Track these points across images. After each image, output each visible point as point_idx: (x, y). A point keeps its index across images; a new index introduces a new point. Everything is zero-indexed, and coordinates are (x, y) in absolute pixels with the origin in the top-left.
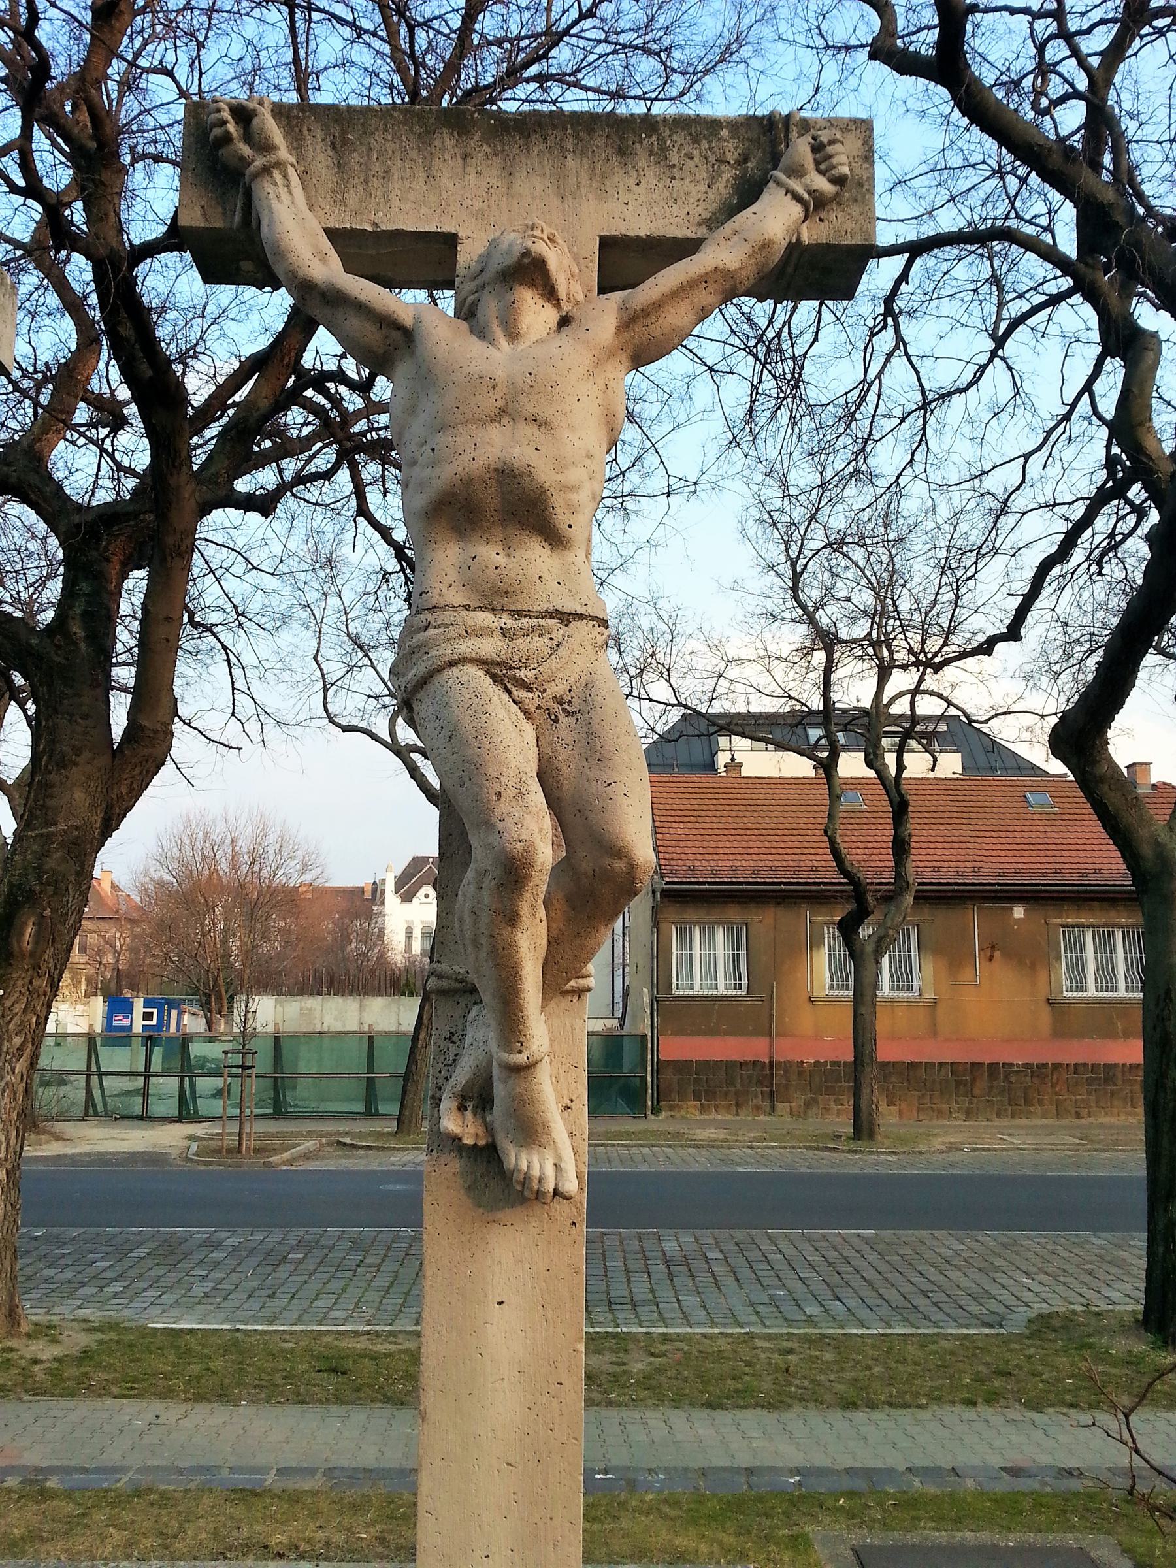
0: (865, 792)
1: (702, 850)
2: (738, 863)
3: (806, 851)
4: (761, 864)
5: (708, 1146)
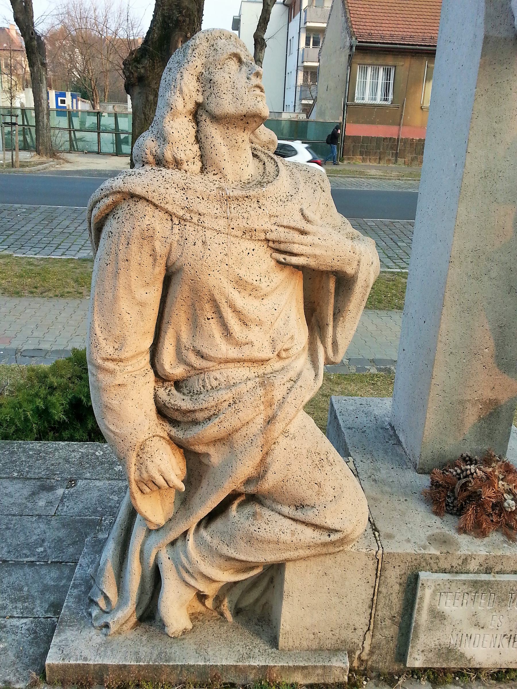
2: (392, 33)
3: (427, 28)
4: (405, 34)
5: (379, 179)
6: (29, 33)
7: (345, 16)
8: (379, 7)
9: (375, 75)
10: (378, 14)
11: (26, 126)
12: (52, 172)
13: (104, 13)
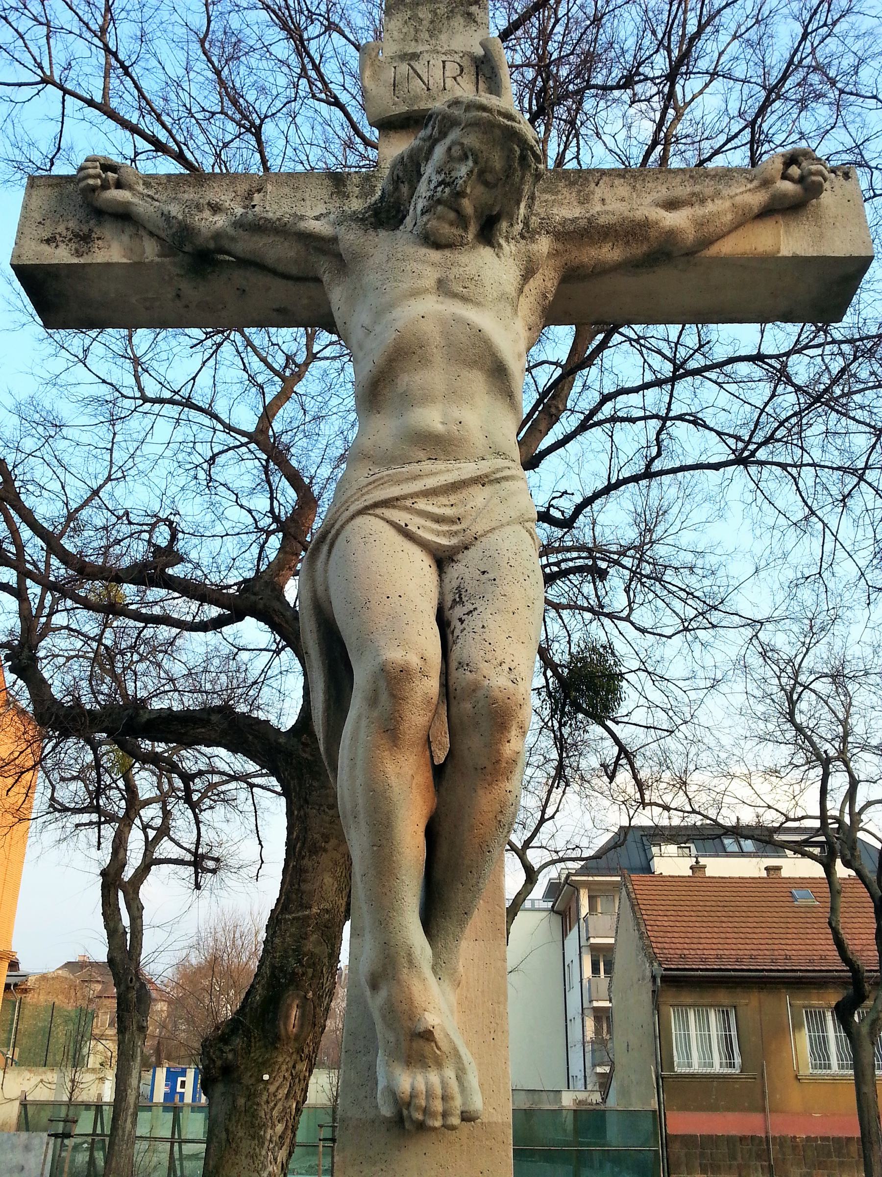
0: (814, 890)
1: (687, 941)
3: (777, 942)
6: (126, 979)
7: (638, 930)
8: (692, 914)
9: (703, 1024)
10: (691, 924)
11: (98, 1135)
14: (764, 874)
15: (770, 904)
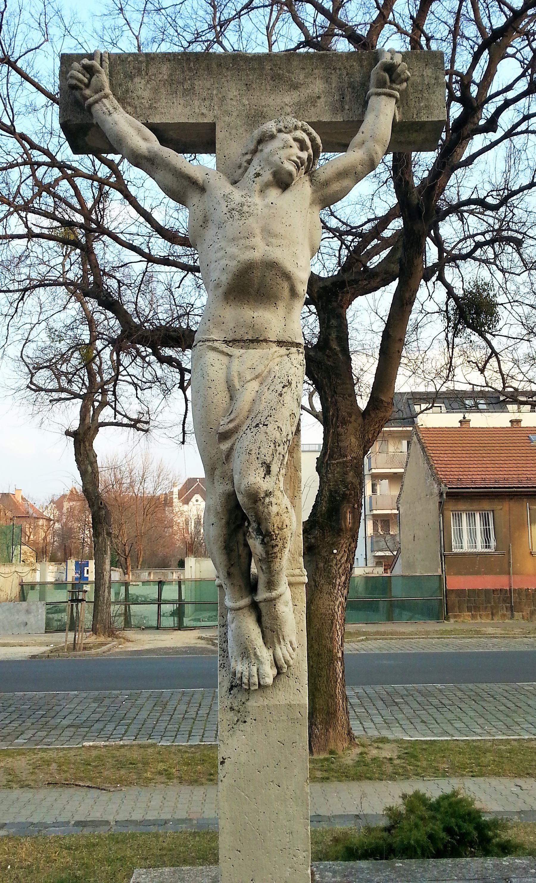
2: (484, 477)
3: (520, 469)
6: (98, 503)
10: (463, 459)
12: (120, 653)
13: (141, 473)
14: (509, 425)
15: (514, 445)
